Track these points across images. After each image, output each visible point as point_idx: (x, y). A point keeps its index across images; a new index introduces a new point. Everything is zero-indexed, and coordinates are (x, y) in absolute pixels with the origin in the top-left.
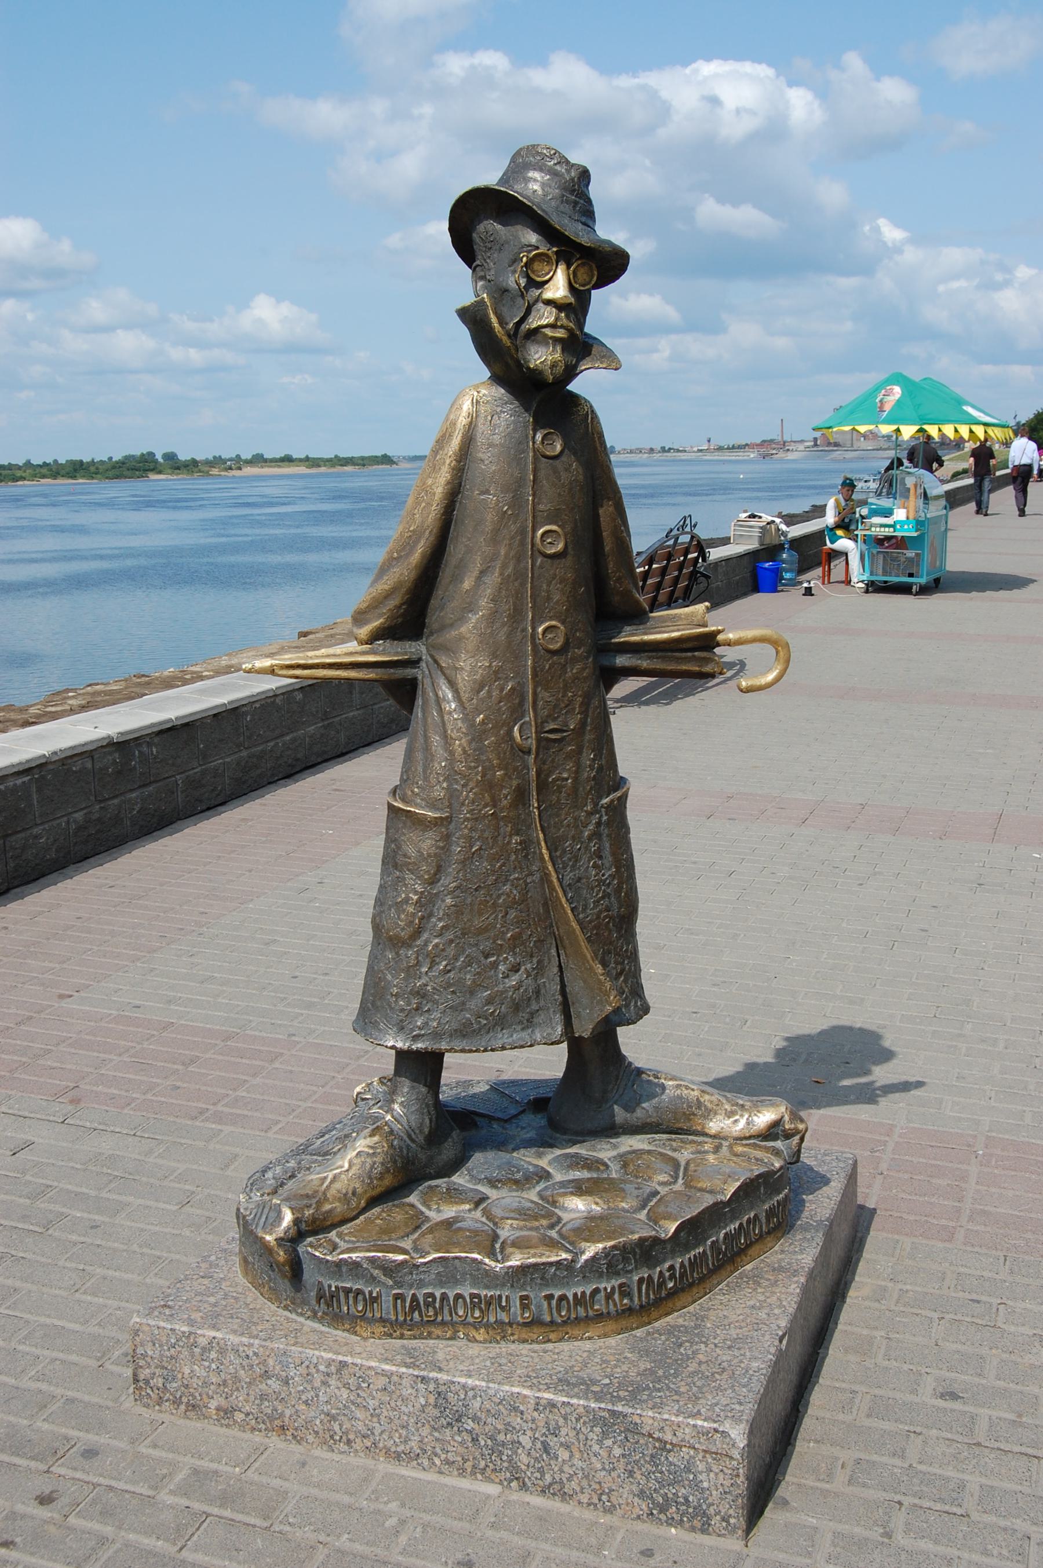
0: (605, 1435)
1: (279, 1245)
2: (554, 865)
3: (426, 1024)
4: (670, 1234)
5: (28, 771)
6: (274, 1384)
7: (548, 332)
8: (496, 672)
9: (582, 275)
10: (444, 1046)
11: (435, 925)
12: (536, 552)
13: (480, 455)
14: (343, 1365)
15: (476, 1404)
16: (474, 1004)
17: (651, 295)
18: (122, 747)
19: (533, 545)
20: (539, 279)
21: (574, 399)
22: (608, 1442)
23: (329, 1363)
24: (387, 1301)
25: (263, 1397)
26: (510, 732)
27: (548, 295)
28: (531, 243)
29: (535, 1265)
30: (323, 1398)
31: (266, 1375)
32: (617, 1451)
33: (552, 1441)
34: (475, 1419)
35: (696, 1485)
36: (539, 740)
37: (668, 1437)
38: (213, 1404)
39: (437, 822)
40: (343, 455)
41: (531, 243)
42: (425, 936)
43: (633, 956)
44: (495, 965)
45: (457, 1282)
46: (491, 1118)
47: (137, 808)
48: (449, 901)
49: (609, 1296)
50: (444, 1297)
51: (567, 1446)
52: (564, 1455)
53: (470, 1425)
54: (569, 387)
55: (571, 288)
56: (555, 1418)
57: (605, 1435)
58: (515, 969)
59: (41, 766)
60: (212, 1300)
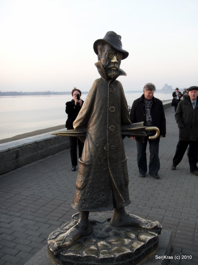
1: (54, 252)
3: (86, 206)
4: (134, 252)
5: (20, 147)
7: (113, 68)
8: (101, 136)
11: (88, 186)
13: (161, 241)
18: (37, 143)
19: (109, 110)
20: (111, 58)
21: (118, 82)
28: (110, 49)
36: (109, 149)
41: (110, 49)
42: (86, 188)
44: (100, 194)
46: (99, 222)
47: (40, 154)
48: (90, 181)
55: (117, 59)
58: (104, 195)
59: (22, 147)
60: (41, 261)
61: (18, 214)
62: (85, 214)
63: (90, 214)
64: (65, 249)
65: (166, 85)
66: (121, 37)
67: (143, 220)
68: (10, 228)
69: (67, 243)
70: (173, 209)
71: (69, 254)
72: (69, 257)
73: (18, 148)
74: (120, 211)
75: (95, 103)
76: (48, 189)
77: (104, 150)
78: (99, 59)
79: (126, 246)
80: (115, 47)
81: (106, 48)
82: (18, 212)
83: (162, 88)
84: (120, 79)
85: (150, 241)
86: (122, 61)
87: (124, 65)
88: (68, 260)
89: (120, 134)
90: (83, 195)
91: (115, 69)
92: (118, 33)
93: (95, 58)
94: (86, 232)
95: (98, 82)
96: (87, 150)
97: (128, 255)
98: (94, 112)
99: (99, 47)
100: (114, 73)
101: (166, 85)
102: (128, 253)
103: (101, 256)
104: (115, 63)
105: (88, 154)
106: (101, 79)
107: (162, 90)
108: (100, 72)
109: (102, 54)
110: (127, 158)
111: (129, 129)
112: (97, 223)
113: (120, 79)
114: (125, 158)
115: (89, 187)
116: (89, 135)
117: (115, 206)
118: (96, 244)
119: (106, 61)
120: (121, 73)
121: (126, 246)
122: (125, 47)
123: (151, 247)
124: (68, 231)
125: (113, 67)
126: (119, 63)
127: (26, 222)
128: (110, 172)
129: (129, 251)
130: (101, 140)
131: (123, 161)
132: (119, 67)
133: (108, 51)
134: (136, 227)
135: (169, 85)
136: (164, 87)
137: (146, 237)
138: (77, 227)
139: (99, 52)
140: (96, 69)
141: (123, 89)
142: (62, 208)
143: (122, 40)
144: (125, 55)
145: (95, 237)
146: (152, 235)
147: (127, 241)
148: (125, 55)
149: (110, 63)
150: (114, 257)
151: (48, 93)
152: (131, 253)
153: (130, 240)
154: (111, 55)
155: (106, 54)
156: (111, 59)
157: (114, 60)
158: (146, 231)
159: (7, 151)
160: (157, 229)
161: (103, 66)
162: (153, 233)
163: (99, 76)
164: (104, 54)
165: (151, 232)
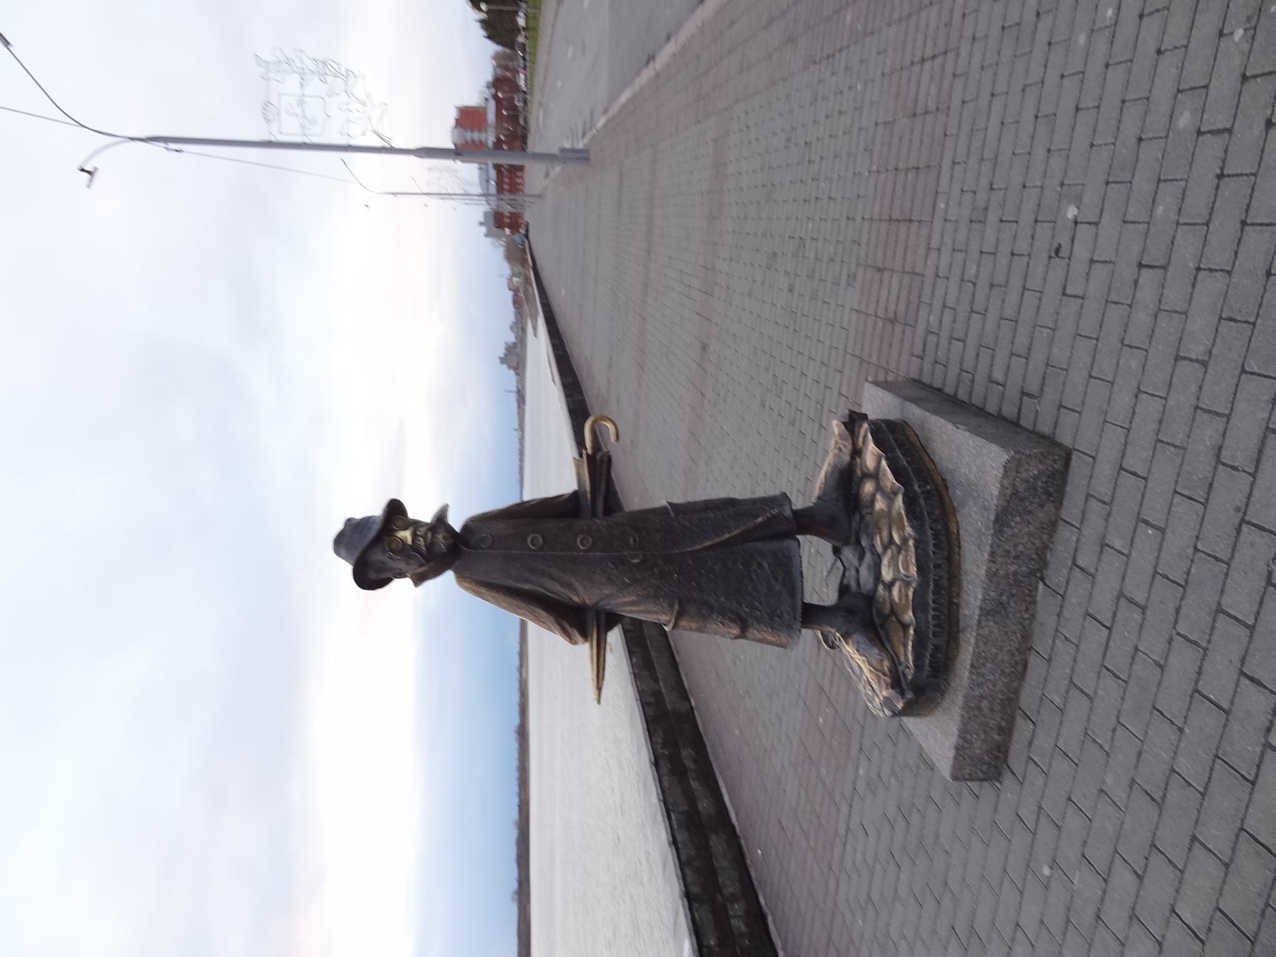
0: (1009, 526)
2: (710, 547)
6: (985, 704)
9: (399, 523)
10: (799, 605)
12: (541, 549)
14: (972, 666)
15: (993, 594)
16: (778, 587)
17: (819, 498)
21: (466, 528)
22: (1013, 524)
23: (971, 673)
24: (936, 641)
25: (992, 710)
26: (634, 565)
27: (409, 541)
28: (382, 548)
29: (917, 560)
30: (991, 677)
31: (979, 708)
32: (1018, 519)
33: (1013, 553)
34: (1001, 595)
35: (1035, 477)
37: (1009, 492)
38: (997, 737)
39: (681, 604)
40: (515, 885)
41: (382, 548)
43: (754, 501)
45: (927, 603)
48: (723, 599)
49: (935, 521)
50: (934, 609)
51: (1016, 545)
52: (1020, 548)
53: (1004, 598)
54: (457, 528)
55: (405, 529)
56: (1000, 552)
57: (1009, 526)
58: (760, 565)
61: (844, 809)
62: (811, 615)
63: (811, 598)
64: (900, 668)
65: (503, 360)
66: (349, 520)
67: (830, 458)
68: (1160, 944)
69: (886, 664)
70: (824, 369)
71: (910, 657)
72: (918, 657)
73: (669, 818)
74: (806, 522)
75: (519, 585)
76: (781, 722)
77: (643, 561)
78: (401, 575)
79: (890, 506)
80: (372, 534)
81: (378, 556)
82: (838, 809)
83: (512, 373)
84: (456, 522)
85: (877, 444)
86: (412, 515)
87: (421, 510)
88: (927, 661)
89: (600, 522)
90: (758, 620)
91: (429, 535)
92: (339, 526)
93: (401, 587)
94: (861, 614)
95: (462, 577)
96: (642, 608)
97: (910, 501)
98: (541, 590)
99: (373, 576)
100: (440, 537)
101: (503, 360)
102: (904, 502)
103: (913, 570)
104: (414, 535)
105: (651, 606)
106: (456, 572)
107: (517, 374)
108: (436, 572)
109: (392, 569)
110: (664, 503)
111: (589, 496)
112: (845, 582)
113: (456, 522)
114: (665, 508)
115: (739, 604)
116: (602, 603)
117: (791, 535)
118: (889, 586)
119: (410, 557)
120: (441, 519)
121: (890, 506)
122: (374, 508)
123: (895, 440)
124: (856, 658)
125: (425, 539)
126: (416, 524)
127: (861, 785)
128: (698, 547)
129: (900, 499)
130: (615, 571)
131: (672, 514)
132: (426, 524)
133: (384, 551)
134: (847, 480)
135: (501, 352)
136: (510, 367)
137: (871, 453)
138: (846, 636)
139: (384, 576)
140: (430, 584)
141: (484, 514)
142: (827, 681)
143: (359, 515)
144: (395, 509)
145: (875, 589)
146: (865, 437)
147: (880, 505)
148: (395, 509)
149: (414, 547)
150: (915, 540)
151: (522, 733)
152: (905, 495)
153: (878, 497)
154: (394, 546)
155: (391, 558)
156: (403, 542)
157: (406, 535)
158: (857, 452)
159: (677, 850)
160: (853, 421)
161: (422, 565)
162: (862, 433)
163: (449, 575)
164: (391, 564)
165: (861, 440)
